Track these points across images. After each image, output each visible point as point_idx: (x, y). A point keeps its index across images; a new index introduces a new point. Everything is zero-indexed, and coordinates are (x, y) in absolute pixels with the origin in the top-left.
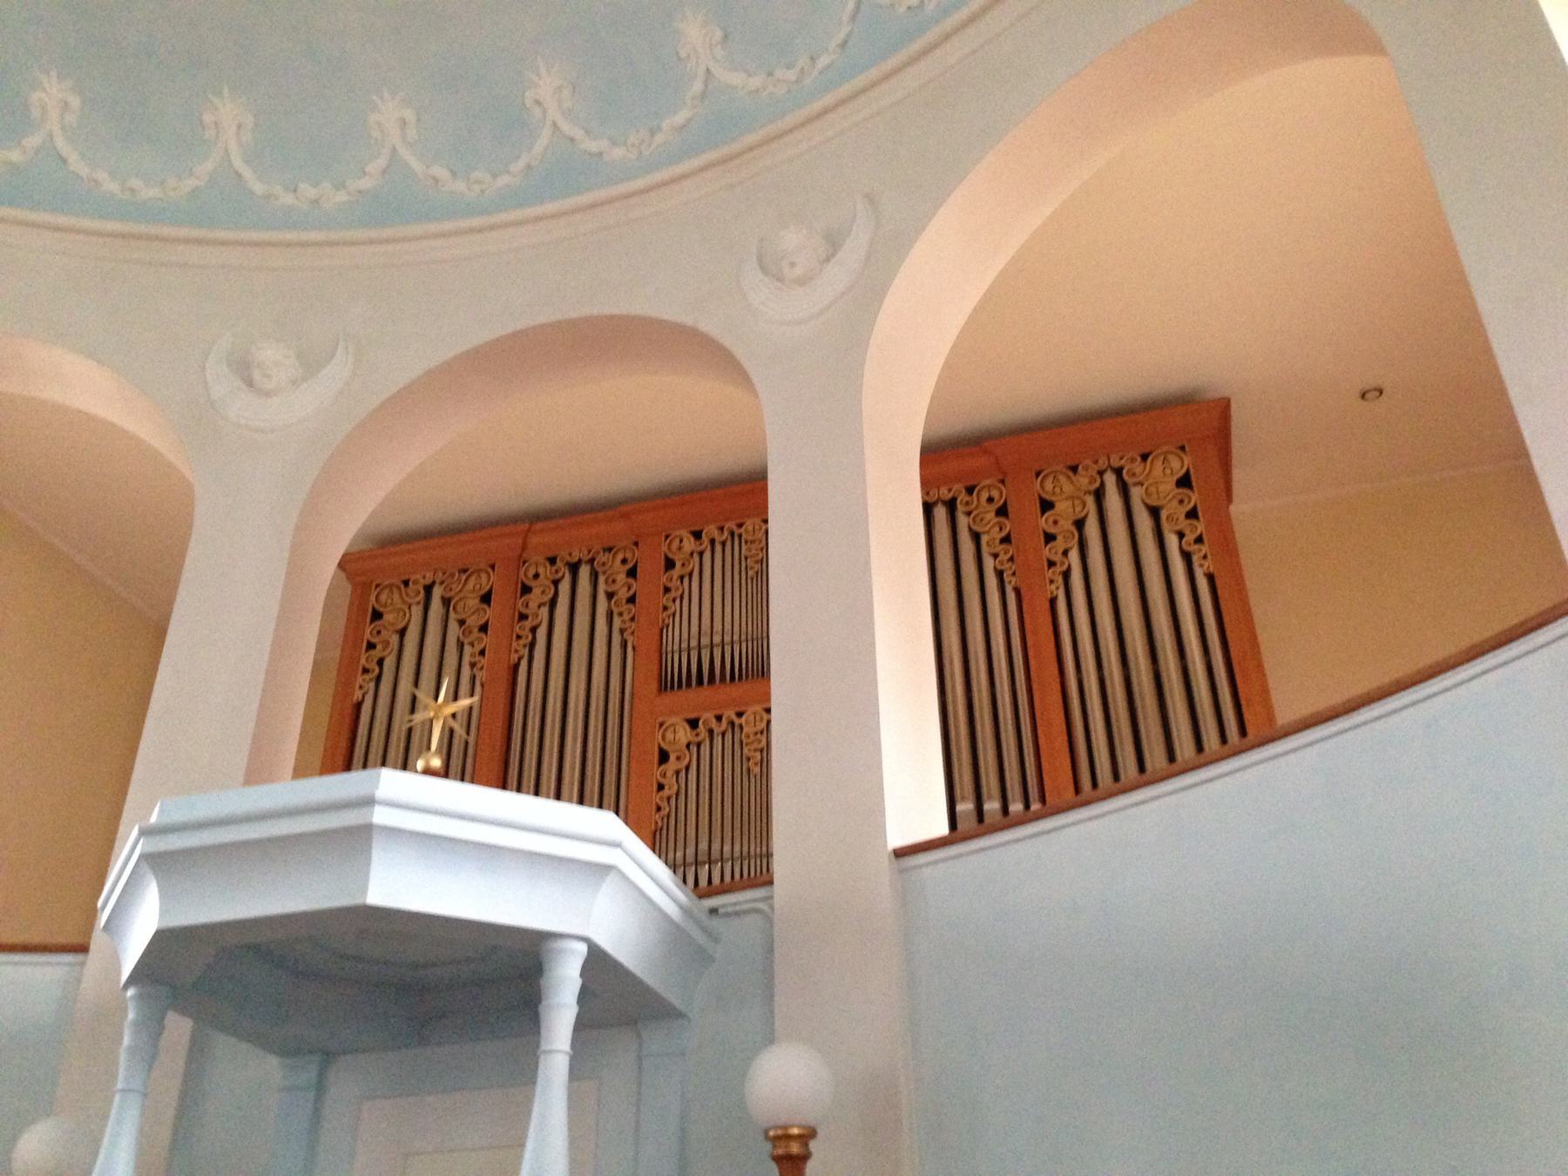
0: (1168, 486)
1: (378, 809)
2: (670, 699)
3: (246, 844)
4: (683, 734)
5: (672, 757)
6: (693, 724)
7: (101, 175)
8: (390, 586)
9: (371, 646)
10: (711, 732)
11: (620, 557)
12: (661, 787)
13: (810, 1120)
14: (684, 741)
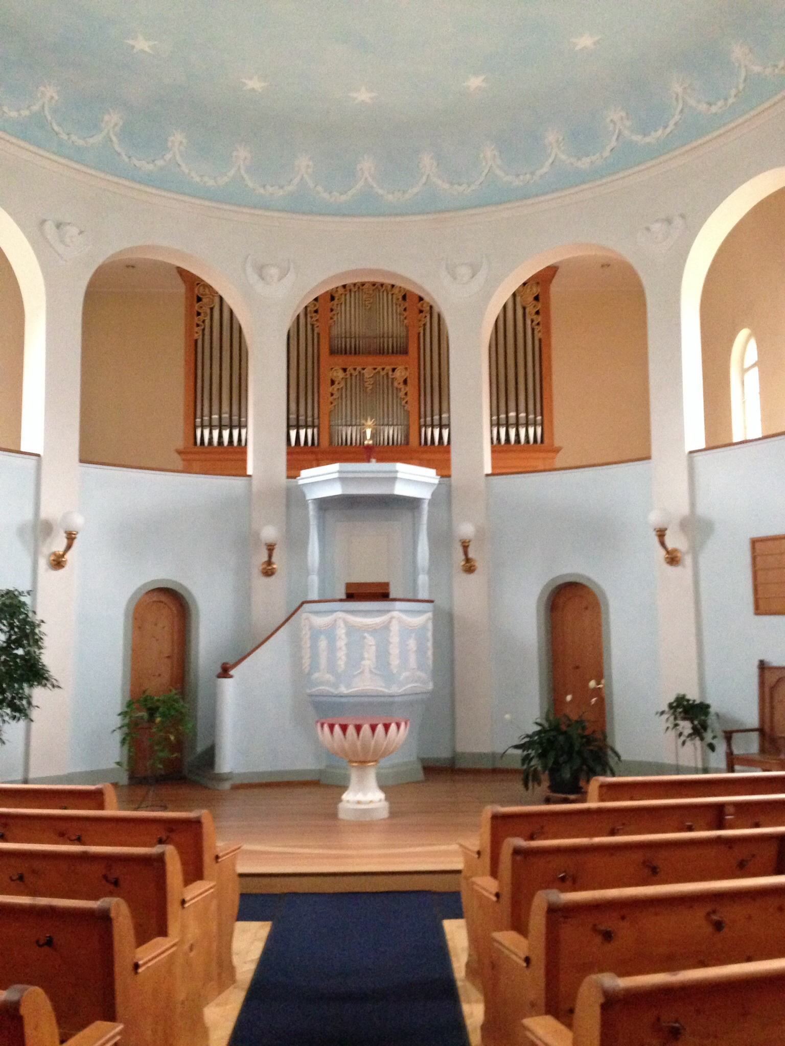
0: (531, 299)
4: (341, 374)
6: (345, 370)
7: (193, 174)
9: (199, 314)
10: (351, 375)
12: (332, 395)
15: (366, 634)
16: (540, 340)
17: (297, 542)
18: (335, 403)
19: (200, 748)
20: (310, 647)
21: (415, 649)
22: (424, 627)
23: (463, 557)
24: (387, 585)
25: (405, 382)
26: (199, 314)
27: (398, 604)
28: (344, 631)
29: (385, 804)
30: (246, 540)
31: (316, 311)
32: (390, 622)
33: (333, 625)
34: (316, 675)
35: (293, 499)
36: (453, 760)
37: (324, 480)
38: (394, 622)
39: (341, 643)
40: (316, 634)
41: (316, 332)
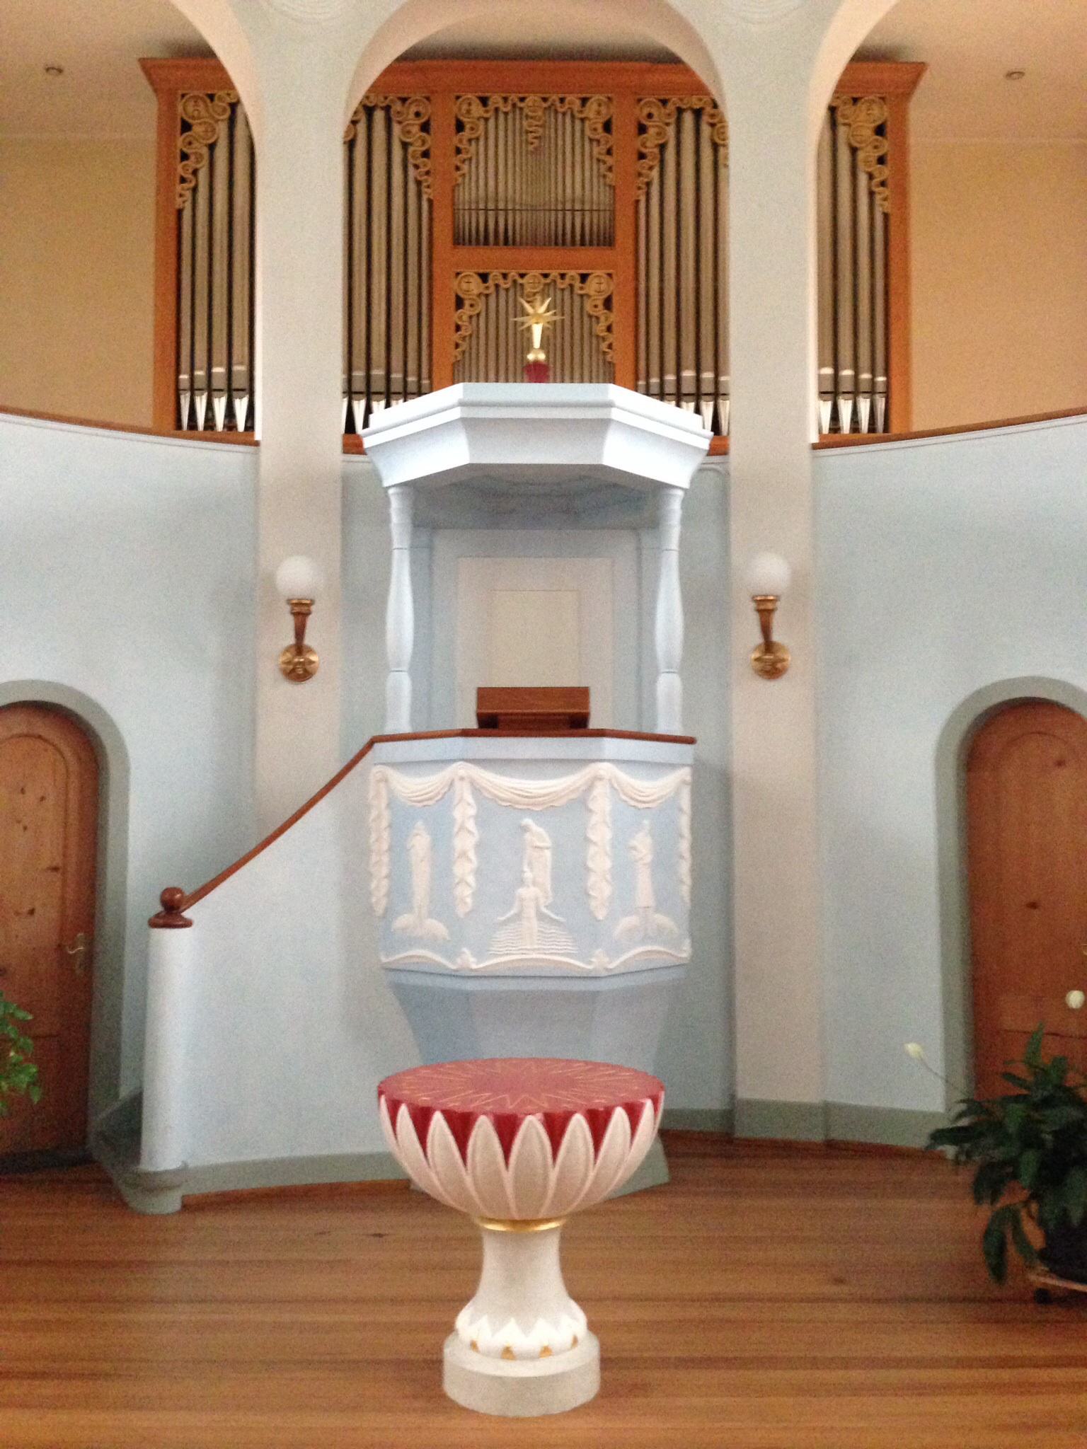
0: (867, 133)
1: (613, 410)
2: (463, 252)
3: (561, 421)
4: (475, 286)
5: (467, 303)
6: (484, 277)
8: (196, 98)
9: (185, 157)
11: (413, 109)
12: (458, 328)
13: (779, 593)
14: (476, 292)
15: (528, 821)
16: (886, 216)
17: (366, 604)
18: (464, 346)
19: (125, 1091)
20: (390, 849)
21: (649, 858)
22: (671, 803)
23: (758, 639)
24: (582, 694)
25: (608, 303)
26: (185, 157)
27: (608, 742)
28: (472, 811)
29: (589, 1349)
30: (243, 594)
31: (426, 154)
32: (590, 787)
33: (446, 798)
34: (403, 921)
35: (356, 501)
36: (729, 1115)
37: (428, 435)
38: (600, 790)
39: (465, 842)
40: (403, 817)
41: (425, 197)
